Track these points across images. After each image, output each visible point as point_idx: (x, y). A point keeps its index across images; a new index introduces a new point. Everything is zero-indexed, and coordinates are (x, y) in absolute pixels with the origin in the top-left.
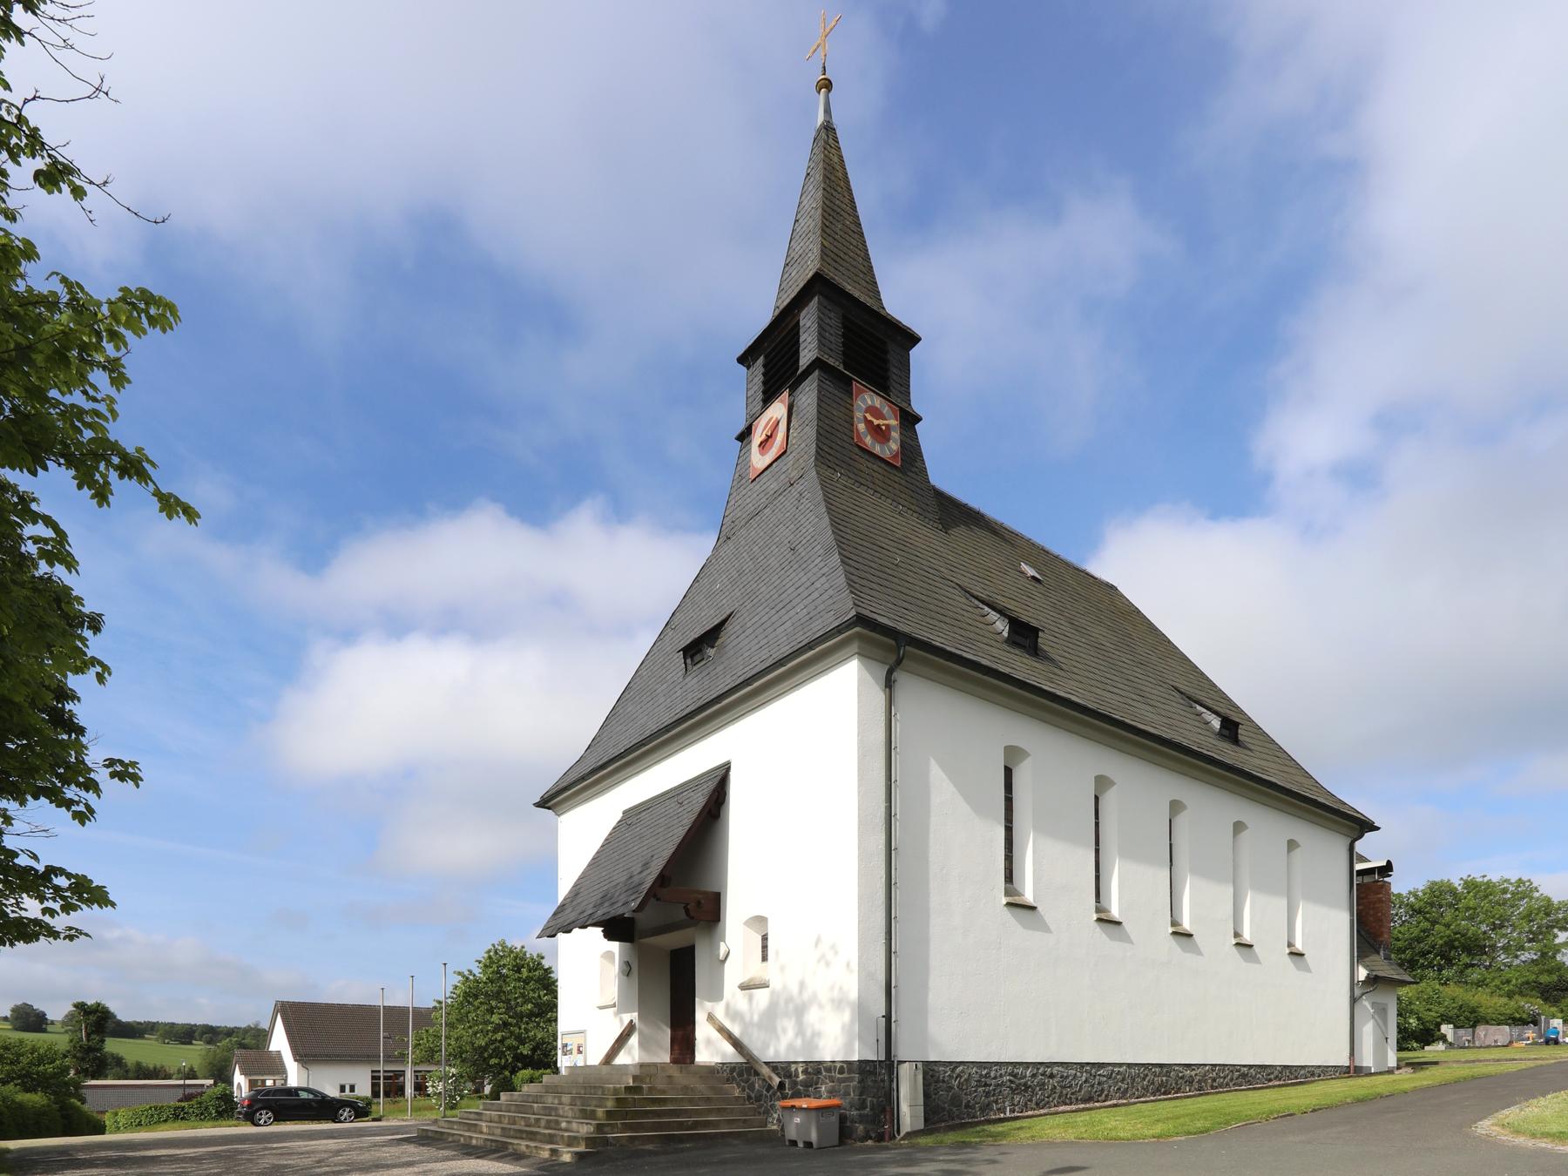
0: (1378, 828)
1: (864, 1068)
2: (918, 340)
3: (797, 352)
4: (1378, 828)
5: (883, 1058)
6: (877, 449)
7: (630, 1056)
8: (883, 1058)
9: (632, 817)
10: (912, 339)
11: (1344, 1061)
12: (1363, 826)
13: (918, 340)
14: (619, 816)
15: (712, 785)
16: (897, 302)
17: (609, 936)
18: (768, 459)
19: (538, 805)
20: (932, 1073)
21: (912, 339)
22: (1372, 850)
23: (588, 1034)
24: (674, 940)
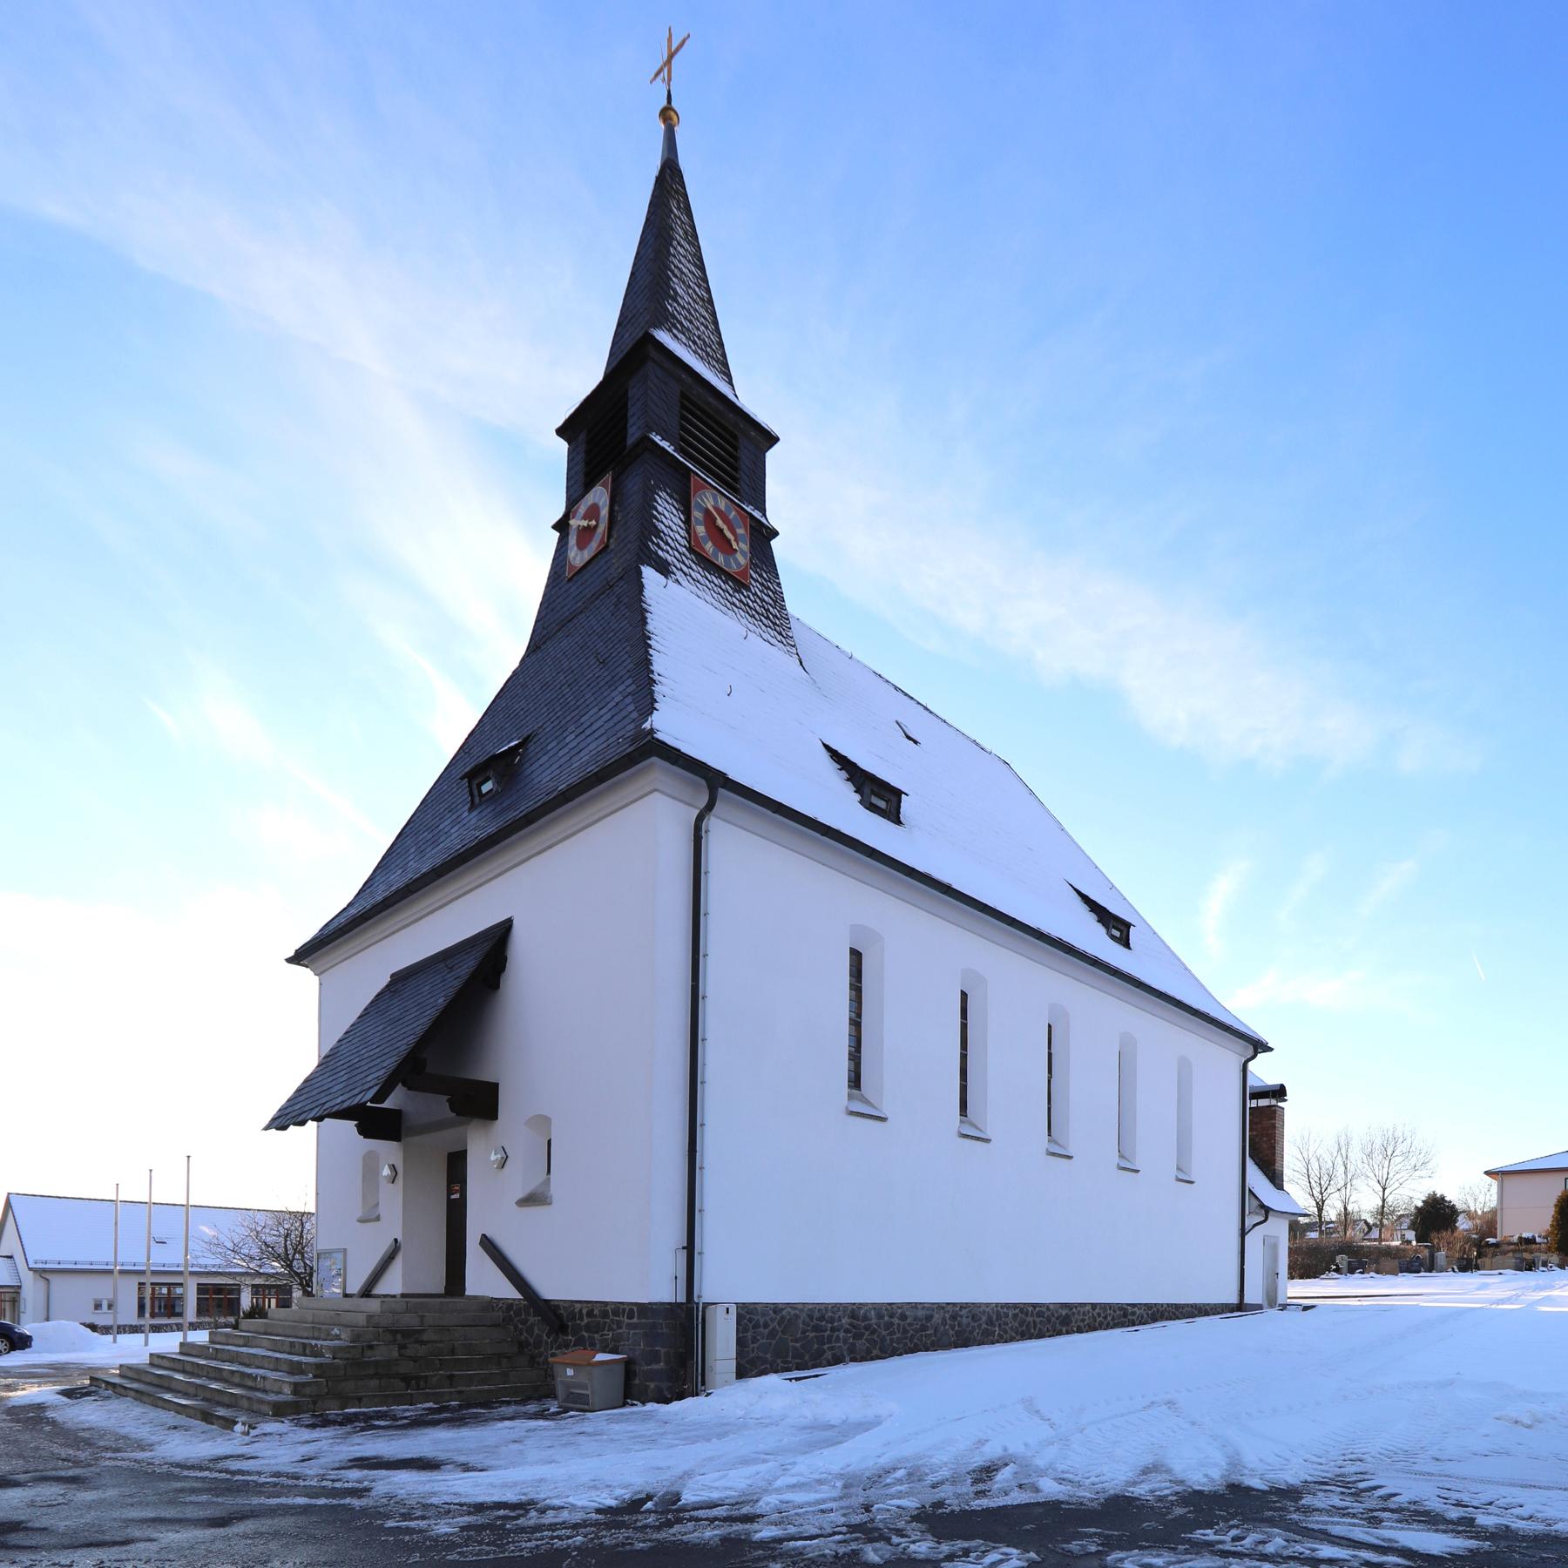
0: (1271, 1049)
1: (670, 1309)
2: (777, 439)
3: (625, 428)
4: (1271, 1049)
5: (682, 1298)
6: (720, 560)
7: (393, 1284)
8: (682, 1298)
9: (401, 980)
10: (772, 440)
11: (1234, 1300)
12: (1259, 1047)
13: (777, 439)
14: (385, 980)
15: (487, 947)
16: (754, 391)
17: (366, 1131)
18: (587, 554)
19: (289, 960)
20: (748, 1315)
21: (772, 440)
22: (1264, 1071)
23: (99, 1297)
24: (445, 1140)
